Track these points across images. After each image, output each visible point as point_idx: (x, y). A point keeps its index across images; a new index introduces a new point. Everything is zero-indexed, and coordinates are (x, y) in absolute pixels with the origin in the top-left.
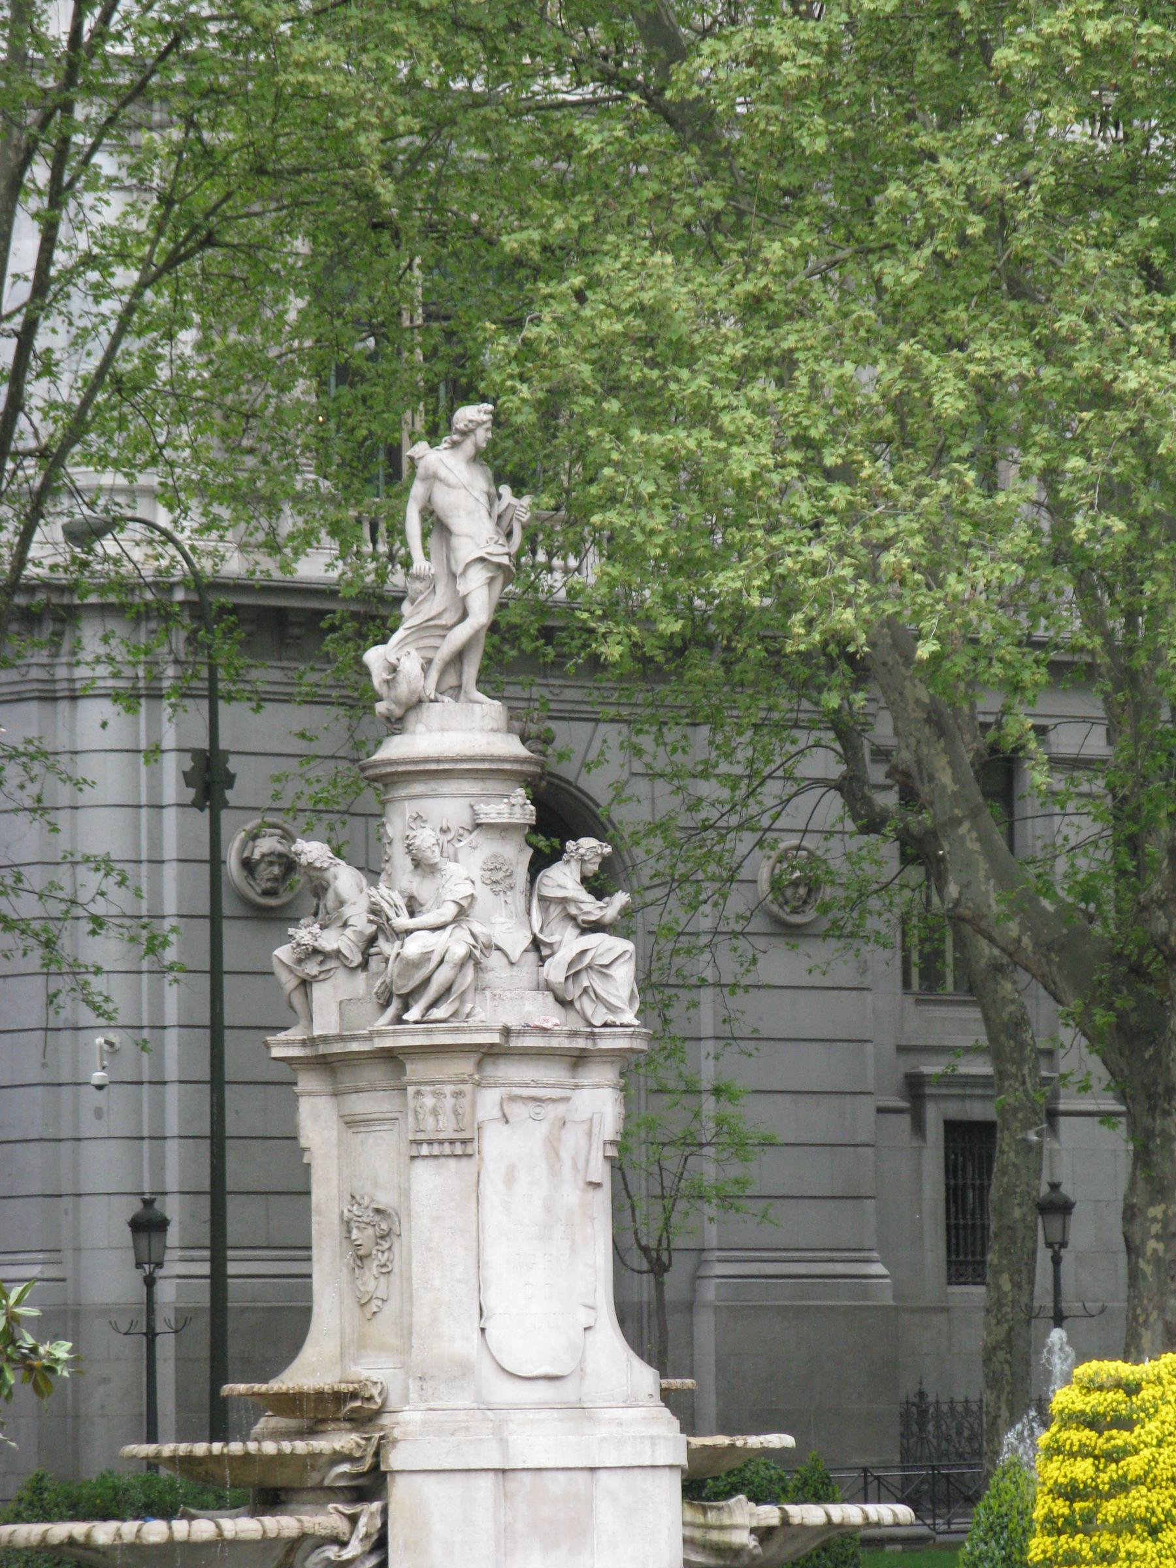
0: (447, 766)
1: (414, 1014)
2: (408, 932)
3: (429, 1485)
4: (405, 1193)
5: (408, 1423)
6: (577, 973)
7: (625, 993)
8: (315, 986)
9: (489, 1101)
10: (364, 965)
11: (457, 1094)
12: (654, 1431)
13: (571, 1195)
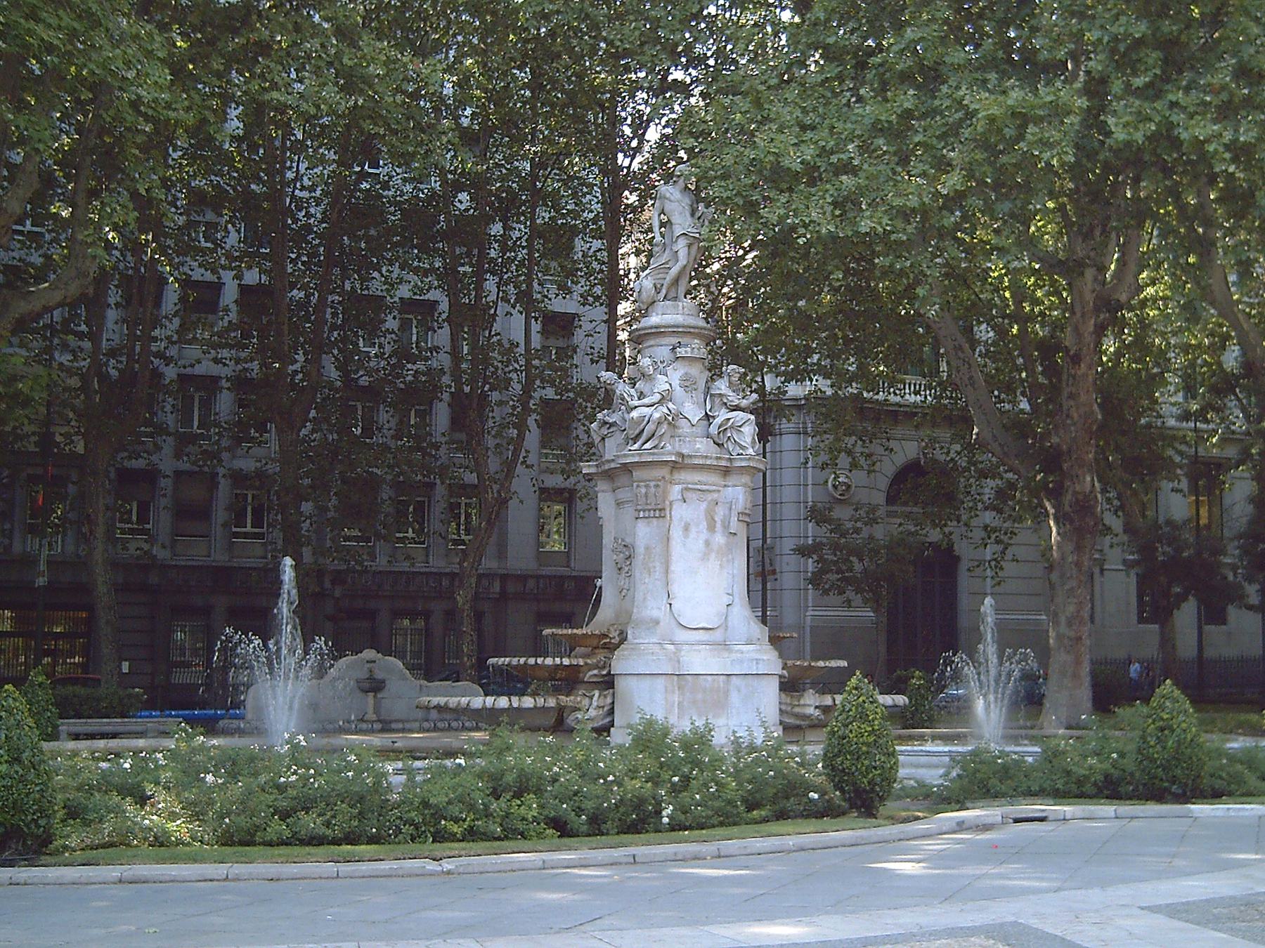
3: (632, 682)
5: (273, 688)
7: (749, 440)
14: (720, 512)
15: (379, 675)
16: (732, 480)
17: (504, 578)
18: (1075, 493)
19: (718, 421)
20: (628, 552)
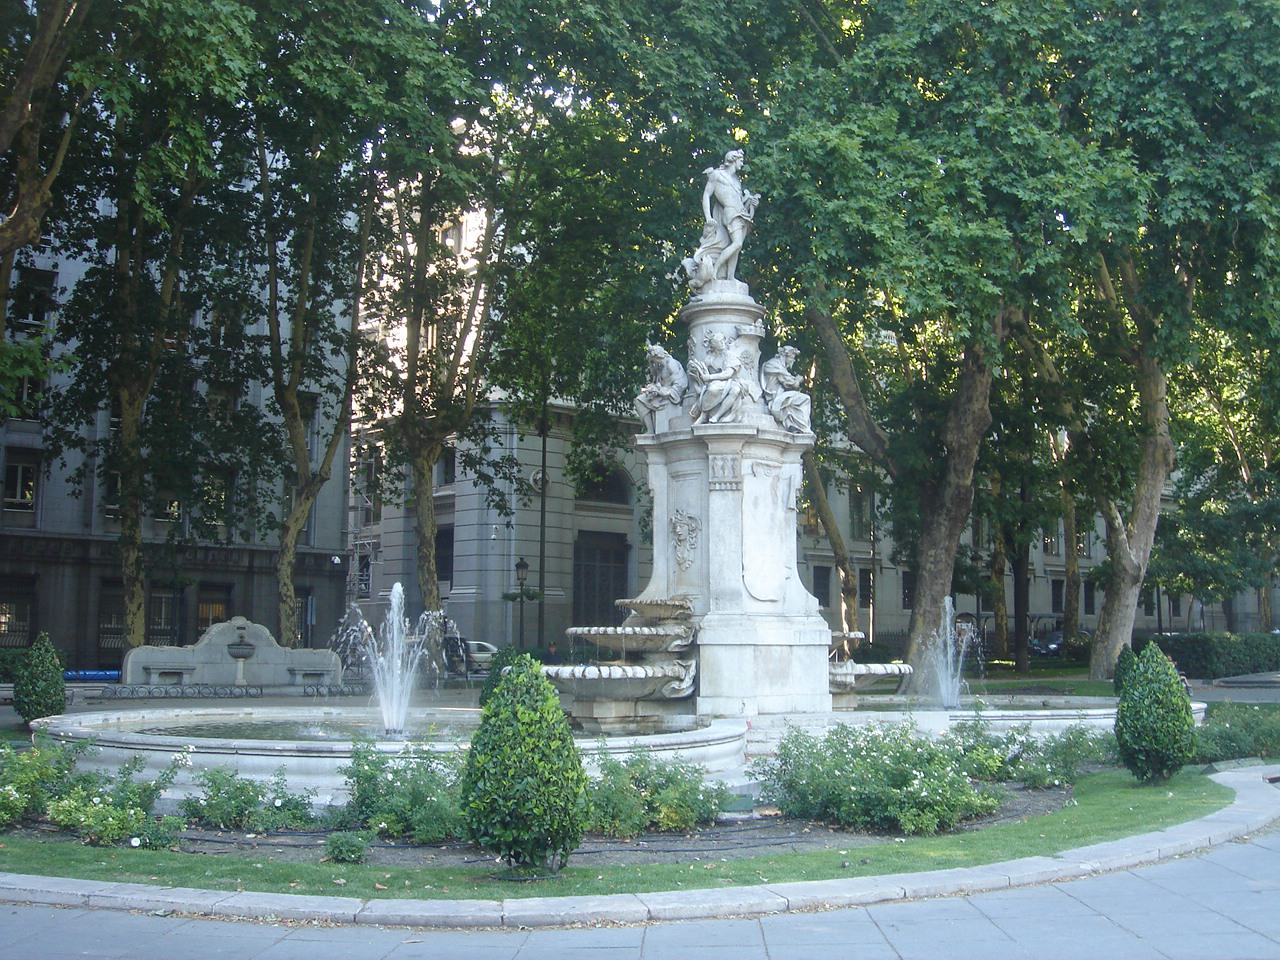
1: (714, 419)
2: (711, 381)
3: (721, 652)
4: (706, 508)
10: (681, 403)
11: (734, 460)
12: (821, 628)
13: (781, 513)
17: (252, 553)
18: (958, 487)
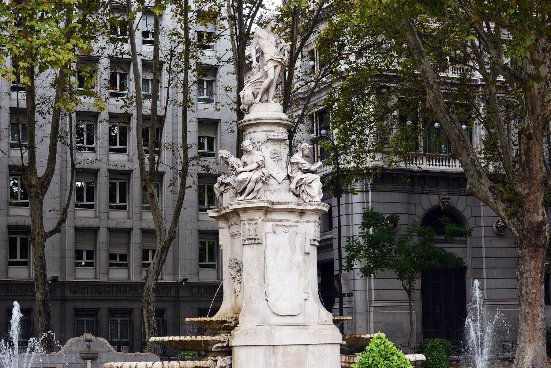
0: (258, 121)
6: (301, 185)
8: (224, 194)
9: (269, 226)
13: (299, 256)
14: (299, 239)
15: (94, 349)
16: (305, 218)
19: (295, 181)
20: (238, 267)
